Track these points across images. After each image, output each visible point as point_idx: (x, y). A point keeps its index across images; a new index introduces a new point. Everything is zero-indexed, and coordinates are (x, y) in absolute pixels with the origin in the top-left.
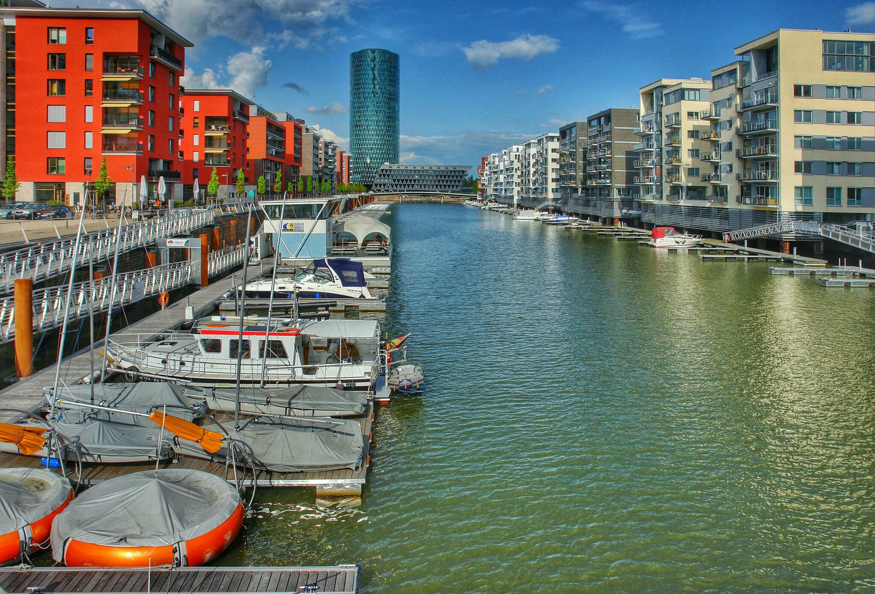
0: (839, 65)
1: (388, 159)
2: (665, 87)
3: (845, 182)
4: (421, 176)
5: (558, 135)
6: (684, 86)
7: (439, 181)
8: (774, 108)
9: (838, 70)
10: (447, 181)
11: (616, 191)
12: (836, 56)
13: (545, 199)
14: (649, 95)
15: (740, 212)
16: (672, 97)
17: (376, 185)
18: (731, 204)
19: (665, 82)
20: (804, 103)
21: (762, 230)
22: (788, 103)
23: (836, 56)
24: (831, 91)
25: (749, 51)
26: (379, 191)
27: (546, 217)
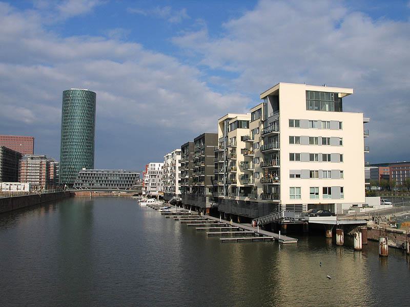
0: (317, 108)
1: (85, 166)
2: (230, 119)
3: (321, 183)
4: (120, 178)
5: (180, 150)
6: (239, 119)
7: (127, 182)
8: (277, 135)
9: (316, 110)
10: (85, 177)
11: (207, 190)
12: (315, 101)
13: (175, 195)
14: (222, 124)
15: (263, 204)
16: (233, 125)
17: (76, 184)
18: (259, 200)
19: (230, 116)
20: (295, 132)
21: (272, 217)
22: (285, 132)
23: (315, 101)
24: (313, 124)
25: (266, 97)
26: (78, 188)
27: (153, 203)
